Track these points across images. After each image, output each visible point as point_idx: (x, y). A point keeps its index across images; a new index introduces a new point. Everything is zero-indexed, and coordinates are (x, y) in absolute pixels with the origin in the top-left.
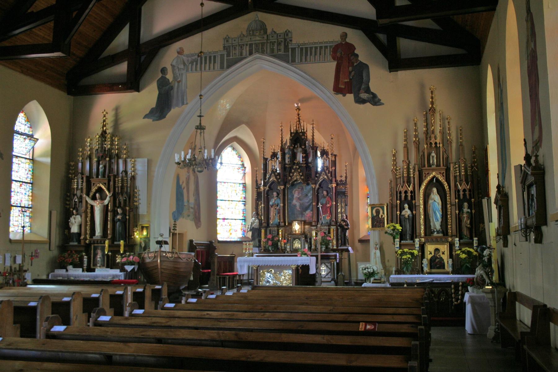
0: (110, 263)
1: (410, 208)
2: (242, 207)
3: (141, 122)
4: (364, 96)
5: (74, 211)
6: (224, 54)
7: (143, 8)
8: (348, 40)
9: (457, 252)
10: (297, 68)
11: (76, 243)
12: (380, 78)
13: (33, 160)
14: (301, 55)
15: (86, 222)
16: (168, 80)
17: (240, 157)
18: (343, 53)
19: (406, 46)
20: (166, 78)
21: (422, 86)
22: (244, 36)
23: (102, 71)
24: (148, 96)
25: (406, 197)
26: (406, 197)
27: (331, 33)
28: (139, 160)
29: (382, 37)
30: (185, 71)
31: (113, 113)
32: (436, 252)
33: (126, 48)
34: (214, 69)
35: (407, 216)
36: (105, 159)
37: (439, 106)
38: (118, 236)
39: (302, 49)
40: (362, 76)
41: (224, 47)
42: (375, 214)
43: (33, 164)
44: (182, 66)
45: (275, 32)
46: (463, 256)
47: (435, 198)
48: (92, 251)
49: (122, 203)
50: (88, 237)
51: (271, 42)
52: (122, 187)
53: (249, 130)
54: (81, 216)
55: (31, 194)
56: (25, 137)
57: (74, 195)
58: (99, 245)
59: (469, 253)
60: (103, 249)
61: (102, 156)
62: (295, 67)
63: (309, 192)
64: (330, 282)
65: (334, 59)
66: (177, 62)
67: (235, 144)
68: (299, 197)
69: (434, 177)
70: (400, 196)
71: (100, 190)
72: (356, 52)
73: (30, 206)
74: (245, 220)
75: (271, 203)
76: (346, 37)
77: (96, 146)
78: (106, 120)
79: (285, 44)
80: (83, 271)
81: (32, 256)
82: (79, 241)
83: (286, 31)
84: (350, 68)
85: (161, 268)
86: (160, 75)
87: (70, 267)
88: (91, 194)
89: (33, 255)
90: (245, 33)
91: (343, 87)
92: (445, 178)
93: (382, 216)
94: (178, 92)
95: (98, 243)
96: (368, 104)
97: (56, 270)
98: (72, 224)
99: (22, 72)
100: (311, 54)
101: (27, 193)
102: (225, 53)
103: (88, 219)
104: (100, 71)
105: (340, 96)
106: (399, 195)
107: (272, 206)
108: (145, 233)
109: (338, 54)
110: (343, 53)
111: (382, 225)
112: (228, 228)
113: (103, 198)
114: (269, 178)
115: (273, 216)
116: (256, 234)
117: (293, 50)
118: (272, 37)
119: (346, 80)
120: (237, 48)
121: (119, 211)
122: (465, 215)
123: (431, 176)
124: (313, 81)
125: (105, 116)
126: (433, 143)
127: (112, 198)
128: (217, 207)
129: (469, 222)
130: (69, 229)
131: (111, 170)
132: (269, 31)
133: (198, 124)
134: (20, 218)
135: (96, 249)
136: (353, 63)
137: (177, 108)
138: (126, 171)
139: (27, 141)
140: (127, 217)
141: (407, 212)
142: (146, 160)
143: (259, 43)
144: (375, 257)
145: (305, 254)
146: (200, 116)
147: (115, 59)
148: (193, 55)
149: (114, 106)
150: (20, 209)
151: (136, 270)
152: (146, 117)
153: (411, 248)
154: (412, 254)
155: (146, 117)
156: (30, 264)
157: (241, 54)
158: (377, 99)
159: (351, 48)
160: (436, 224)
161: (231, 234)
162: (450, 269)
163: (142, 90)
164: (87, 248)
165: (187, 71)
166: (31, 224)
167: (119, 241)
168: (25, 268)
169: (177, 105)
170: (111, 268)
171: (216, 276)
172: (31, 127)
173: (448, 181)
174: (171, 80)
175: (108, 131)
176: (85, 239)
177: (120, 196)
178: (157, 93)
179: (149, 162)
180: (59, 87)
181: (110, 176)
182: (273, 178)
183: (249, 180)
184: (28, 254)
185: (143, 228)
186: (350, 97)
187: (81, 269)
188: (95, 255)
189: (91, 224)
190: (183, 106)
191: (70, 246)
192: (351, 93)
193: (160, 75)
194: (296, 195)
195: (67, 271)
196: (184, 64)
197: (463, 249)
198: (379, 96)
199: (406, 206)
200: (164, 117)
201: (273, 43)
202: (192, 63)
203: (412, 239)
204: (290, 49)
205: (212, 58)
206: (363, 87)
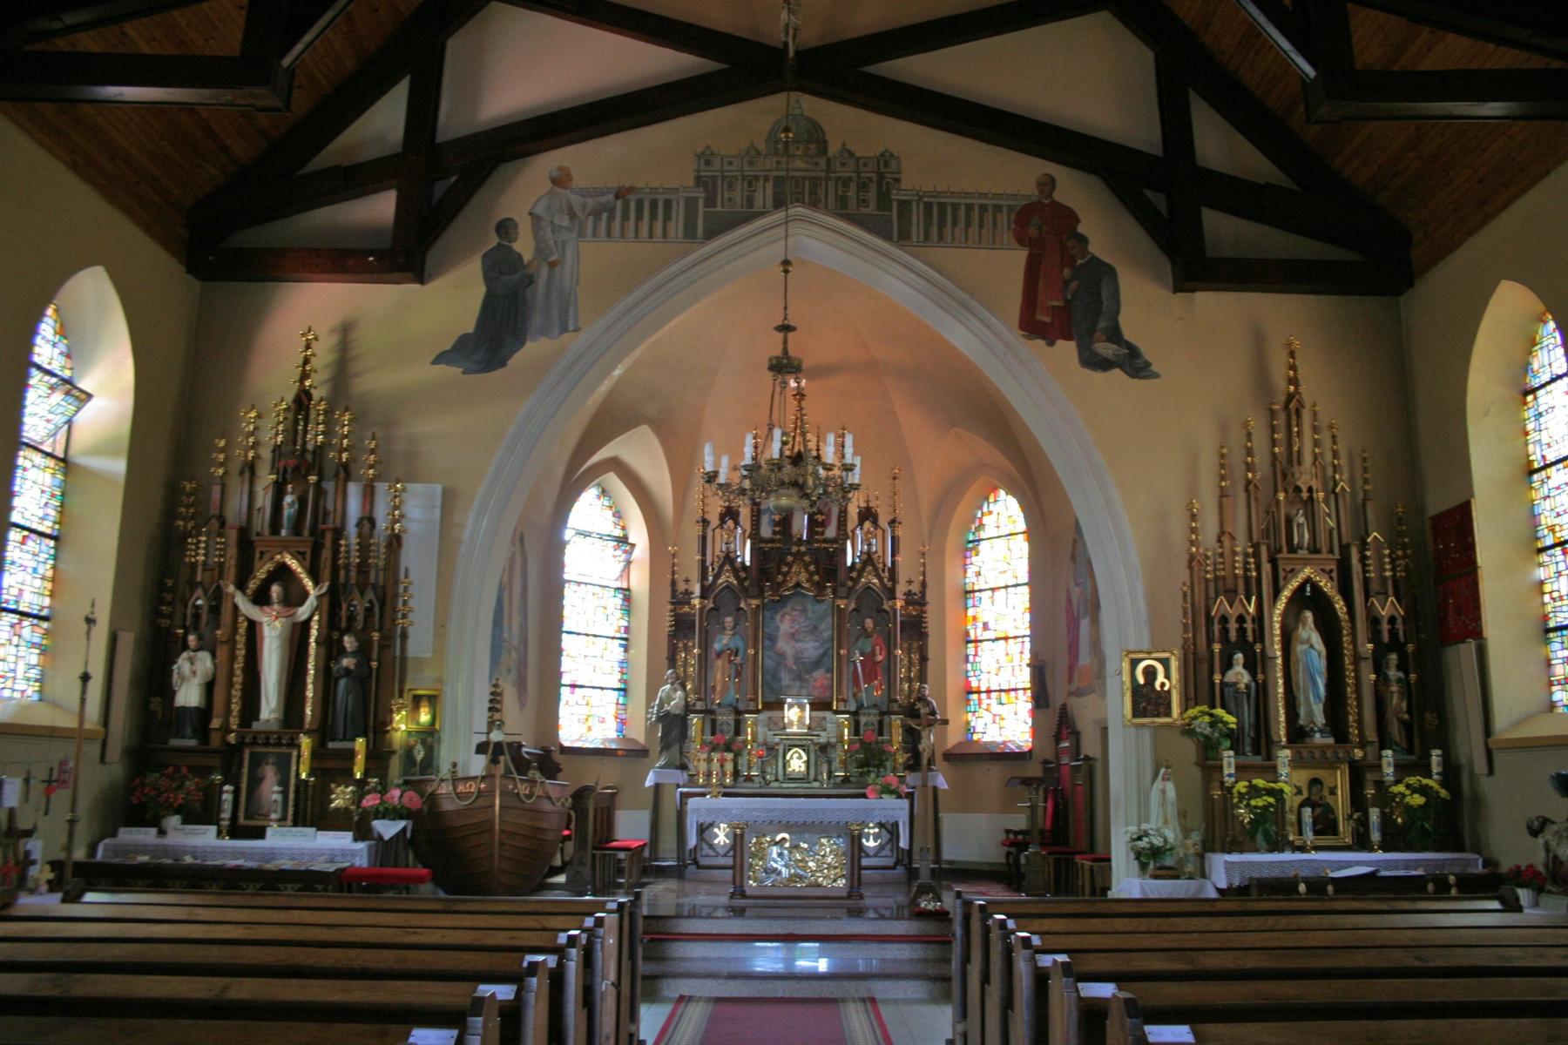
0: (310, 810)
1: (1250, 666)
2: (619, 653)
3: (423, 373)
4: (1105, 349)
5: (192, 638)
6: (696, 199)
7: (452, 44)
10: (916, 257)
11: (192, 743)
12: (1145, 305)
13: (65, 463)
14: (928, 224)
15: (231, 673)
16: (520, 256)
17: (618, 515)
18: (1045, 229)
19: (1222, 229)
20: (511, 250)
21: (1258, 338)
22: (759, 153)
23: (297, 218)
24: (453, 298)
25: (1242, 631)
26: (1242, 631)
27: (1013, 174)
28: (415, 487)
30: (574, 235)
31: (334, 340)
32: (1315, 790)
33: (399, 150)
34: (665, 236)
36: (305, 477)
37: (1307, 393)
38: (340, 723)
39: (928, 206)
40: (1099, 294)
41: (698, 178)
42: (1141, 681)
43: (65, 474)
44: (565, 222)
45: (851, 154)
48: (245, 770)
49: (360, 618)
50: (234, 722)
51: (838, 178)
52: (363, 568)
53: (655, 443)
54: (214, 656)
55: (50, 574)
56: (54, 380)
57: (193, 585)
58: (271, 749)
59: (1423, 790)
60: (283, 765)
61: (296, 469)
62: (911, 254)
64: (894, 868)
65: (1021, 241)
67: (612, 480)
68: (797, 632)
69: (1308, 580)
71: (282, 573)
72: (1081, 229)
73: (44, 613)
74: (624, 690)
75: (717, 646)
76: (1054, 188)
77: (272, 435)
78: (313, 359)
79: (879, 191)
80: (219, 833)
81: (49, 782)
82: (203, 732)
83: (883, 155)
84: (1067, 272)
85: (502, 831)
86: (494, 240)
87: (174, 821)
88: (253, 585)
89: (55, 777)
90: (761, 147)
91: (1047, 320)
92: (1335, 584)
93: (1163, 685)
94: (548, 294)
95: (267, 744)
96: (1117, 373)
97: (122, 830)
98: (183, 678)
99: (74, 167)
100: (955, 224)
101: (41, 570)
102: (701, 196)
103: (239, 665)
104: (298, 212)
105: (1040, 343)
107: (719, 655)
108: (425, 717)
109: (1033, 231)
110: (1045, 230)
111: (1162, 709)
112: (585, 710)
113: (294, 597)
114: (717, 577)
115: (724, 683)
116: (674, 734)
117: (904, 206)
118: (843, 164)
119: (1056, 303)
120: (739, 185)
121: (349, 642)
122: (1394, 688)
124: (963, 295)
125: (308, 347)
126: (1304, 489)
127: (326, 601)
128: (559, 651)
129: (1404, 705)
130: (171, 694)
131: (320, 514)
132: (834, 148)
133: (778, 352)
134: (13, 650)
135: (257, 761)
137: (543, 341)
138: (368, 520)
139: (58, 397)
140: (374, 664)
142: (438, 488)
143: (804, 178)
144: (1163, 804)
145: (891, 792)
146: (786, 328)
147: (357, 179)
148: (599, 192)
149: (336, 319)
150: (14, 618)
151: (409, 835)
152: (440, 359)
155: (440, 359)
156: (43, 807)
157: (750, 204)
159: (1066, 219)
161: (589, 729)
162: (1348, 840)
163: (432, 277)
164: (229, 759)
165: (581, 234)
166: (43, 674)
167: (353, 740)
168: (23, 824)
169: (545, 332)
170: (320, 828)
171: (590, 851)
172: (68, 356)
173: (1345, 590)
174: (527, 256)
175: (316, 394)
176: (226, 729)
177: (357, 594)
178: (479, 291)
179: (449, 500)
180: (166, 241)
181: (317, 538)
182: (727, 578)
183: (640, 581)
184: (40, 773)
185: (417, 701)
186: (1067, 350)
187: (214, 829)
188: (256, 781)
189: (244, 683)
190: (566, 336)
191: (168, 750)
192: (1068, 338)
193: (494, 240)
195: (162, 833)
196: (572, 215)
198: (1148, 352)
199: (1239, 657)
200: (503, 364)
201: (846, 183)
202: (596, 214)
204: (895, 205)
205: (661, 204)
206: (1102, 324)
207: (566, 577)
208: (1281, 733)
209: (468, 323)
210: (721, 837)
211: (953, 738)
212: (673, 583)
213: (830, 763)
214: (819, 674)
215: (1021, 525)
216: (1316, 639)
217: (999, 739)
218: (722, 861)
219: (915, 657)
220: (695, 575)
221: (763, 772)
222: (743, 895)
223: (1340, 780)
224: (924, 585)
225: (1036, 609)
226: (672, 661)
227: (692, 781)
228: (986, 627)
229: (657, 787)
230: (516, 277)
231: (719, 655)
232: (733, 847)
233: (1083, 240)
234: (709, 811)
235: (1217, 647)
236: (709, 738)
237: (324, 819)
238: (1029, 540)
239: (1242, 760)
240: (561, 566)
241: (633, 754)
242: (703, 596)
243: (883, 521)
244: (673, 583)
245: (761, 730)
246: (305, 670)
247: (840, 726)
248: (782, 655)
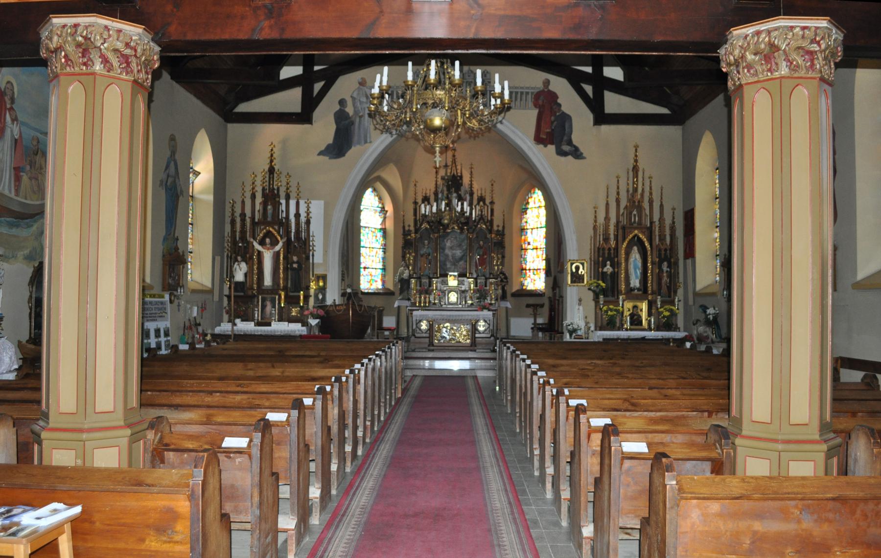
0: (283, 317)
4: (566, 148)
8: (551, 88)
17: (380, 199)
19: (614, 103)
20: (344, 111)
25: (609, 254)
29: (589, 89)
42: (574, 270)
46: (667, 314)
47: (636, 256)
63: (463, 241)
65: (536, 105)
66: (358, 94)
67: (379, 185)
69: (636, 235)
70: (604, 254)
71: (268, 234)
84: (553, 118)
91: (544, 137)
96: (570, 157)
105: (542, 146)
107: (422, 256)
109: (540, 102)
113: (275, 243)
114: (421, 225)
116: (405, 287)
136: (555, 113)
137: (358, 147)
152: (320, 154)
155: (320, 154)
159: (553, 97)
160: (635, 282)
169: (359, 143)
178: (333, 127)
183: (390, 225)
186: (552, 148)
187: (253, 323)
192: (552, 143)
193: (338, 107)
194: (448, 244)
198: (582, 149)
200: (344, 155)
206: (565, 138)
207: (362, 224)
208: (623, 287)
209: (330, 140)
210: (424, 326)
211: (515, 288)
212: (404, 227)
213: (465, 298)
214: (461, 263)
215: (543, 203)
216: (638, 256)
217: (533, 288)
218: (424, 335)
219: (500, 256)
220: (412, 225)
221: (440, 301)
222: (433, 345)
223: (644, 306)
224: (504, 227)
225: (547, 237)
226: (404, 257)
227: (414, 304)
228: (529, 244)
229: (399, 307)
230: (347, 122)
231: (422, 256)
232: (429, 330)
233: (560, 105)
234: (420, 316)
235: (601, 259)
236: (418, 288)
237: (291, 320)
238: (546, 209)
239: (607, 299)
240: (359, 220)
241: (386, 293)
242: (416, 232)
243: (488, 201)
244: (404, 227)
245: (439, 285)
246: (279, 269)
247: (470, 283)
248: (447, 256)
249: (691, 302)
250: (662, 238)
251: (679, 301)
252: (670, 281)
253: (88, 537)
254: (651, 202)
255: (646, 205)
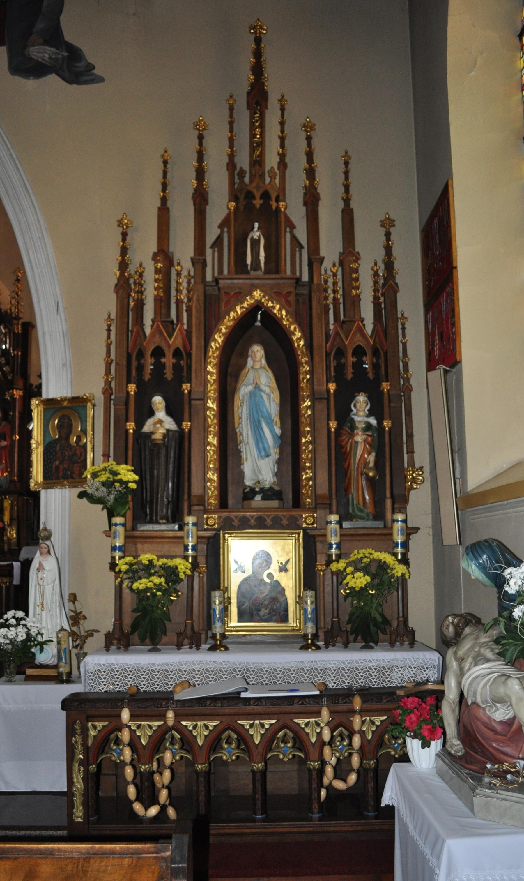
4: (40, 53)
9: (334, 567)
26: (159, 367)
35: (158, 436)
46: (359, 580)
47: (258, 378)
69: (257, 307)
70: (140, 368)
96: (53, 79)
106: (134, 364)
122: (359, 438)
123: (248, 302)
126: (258, 195)
129: (371, 458)
141: (160, 422)
153: (166, 548)
154: (171, 574)
158: (82, 64)
160: (259, 467)
169: (439, 752)
197: (356, 555)
198: (91, 55)
199: (158, 400)
203: (176, 517)
206: (40, 25)
249: (451, 536)
250: (350, 321)
251: (410, 532)
252: (379, 464)
253: (471, 554)
254: (311, 200)
255: (294, 209)
